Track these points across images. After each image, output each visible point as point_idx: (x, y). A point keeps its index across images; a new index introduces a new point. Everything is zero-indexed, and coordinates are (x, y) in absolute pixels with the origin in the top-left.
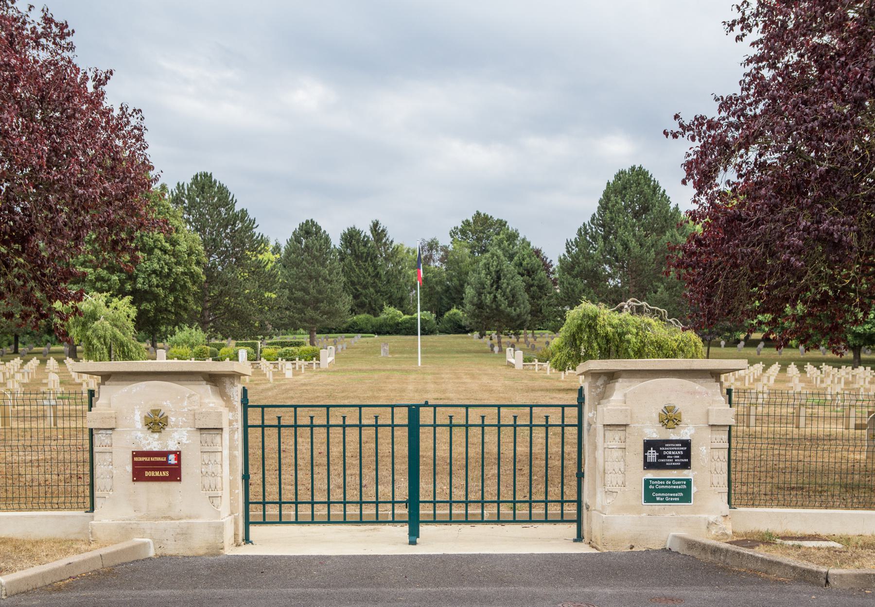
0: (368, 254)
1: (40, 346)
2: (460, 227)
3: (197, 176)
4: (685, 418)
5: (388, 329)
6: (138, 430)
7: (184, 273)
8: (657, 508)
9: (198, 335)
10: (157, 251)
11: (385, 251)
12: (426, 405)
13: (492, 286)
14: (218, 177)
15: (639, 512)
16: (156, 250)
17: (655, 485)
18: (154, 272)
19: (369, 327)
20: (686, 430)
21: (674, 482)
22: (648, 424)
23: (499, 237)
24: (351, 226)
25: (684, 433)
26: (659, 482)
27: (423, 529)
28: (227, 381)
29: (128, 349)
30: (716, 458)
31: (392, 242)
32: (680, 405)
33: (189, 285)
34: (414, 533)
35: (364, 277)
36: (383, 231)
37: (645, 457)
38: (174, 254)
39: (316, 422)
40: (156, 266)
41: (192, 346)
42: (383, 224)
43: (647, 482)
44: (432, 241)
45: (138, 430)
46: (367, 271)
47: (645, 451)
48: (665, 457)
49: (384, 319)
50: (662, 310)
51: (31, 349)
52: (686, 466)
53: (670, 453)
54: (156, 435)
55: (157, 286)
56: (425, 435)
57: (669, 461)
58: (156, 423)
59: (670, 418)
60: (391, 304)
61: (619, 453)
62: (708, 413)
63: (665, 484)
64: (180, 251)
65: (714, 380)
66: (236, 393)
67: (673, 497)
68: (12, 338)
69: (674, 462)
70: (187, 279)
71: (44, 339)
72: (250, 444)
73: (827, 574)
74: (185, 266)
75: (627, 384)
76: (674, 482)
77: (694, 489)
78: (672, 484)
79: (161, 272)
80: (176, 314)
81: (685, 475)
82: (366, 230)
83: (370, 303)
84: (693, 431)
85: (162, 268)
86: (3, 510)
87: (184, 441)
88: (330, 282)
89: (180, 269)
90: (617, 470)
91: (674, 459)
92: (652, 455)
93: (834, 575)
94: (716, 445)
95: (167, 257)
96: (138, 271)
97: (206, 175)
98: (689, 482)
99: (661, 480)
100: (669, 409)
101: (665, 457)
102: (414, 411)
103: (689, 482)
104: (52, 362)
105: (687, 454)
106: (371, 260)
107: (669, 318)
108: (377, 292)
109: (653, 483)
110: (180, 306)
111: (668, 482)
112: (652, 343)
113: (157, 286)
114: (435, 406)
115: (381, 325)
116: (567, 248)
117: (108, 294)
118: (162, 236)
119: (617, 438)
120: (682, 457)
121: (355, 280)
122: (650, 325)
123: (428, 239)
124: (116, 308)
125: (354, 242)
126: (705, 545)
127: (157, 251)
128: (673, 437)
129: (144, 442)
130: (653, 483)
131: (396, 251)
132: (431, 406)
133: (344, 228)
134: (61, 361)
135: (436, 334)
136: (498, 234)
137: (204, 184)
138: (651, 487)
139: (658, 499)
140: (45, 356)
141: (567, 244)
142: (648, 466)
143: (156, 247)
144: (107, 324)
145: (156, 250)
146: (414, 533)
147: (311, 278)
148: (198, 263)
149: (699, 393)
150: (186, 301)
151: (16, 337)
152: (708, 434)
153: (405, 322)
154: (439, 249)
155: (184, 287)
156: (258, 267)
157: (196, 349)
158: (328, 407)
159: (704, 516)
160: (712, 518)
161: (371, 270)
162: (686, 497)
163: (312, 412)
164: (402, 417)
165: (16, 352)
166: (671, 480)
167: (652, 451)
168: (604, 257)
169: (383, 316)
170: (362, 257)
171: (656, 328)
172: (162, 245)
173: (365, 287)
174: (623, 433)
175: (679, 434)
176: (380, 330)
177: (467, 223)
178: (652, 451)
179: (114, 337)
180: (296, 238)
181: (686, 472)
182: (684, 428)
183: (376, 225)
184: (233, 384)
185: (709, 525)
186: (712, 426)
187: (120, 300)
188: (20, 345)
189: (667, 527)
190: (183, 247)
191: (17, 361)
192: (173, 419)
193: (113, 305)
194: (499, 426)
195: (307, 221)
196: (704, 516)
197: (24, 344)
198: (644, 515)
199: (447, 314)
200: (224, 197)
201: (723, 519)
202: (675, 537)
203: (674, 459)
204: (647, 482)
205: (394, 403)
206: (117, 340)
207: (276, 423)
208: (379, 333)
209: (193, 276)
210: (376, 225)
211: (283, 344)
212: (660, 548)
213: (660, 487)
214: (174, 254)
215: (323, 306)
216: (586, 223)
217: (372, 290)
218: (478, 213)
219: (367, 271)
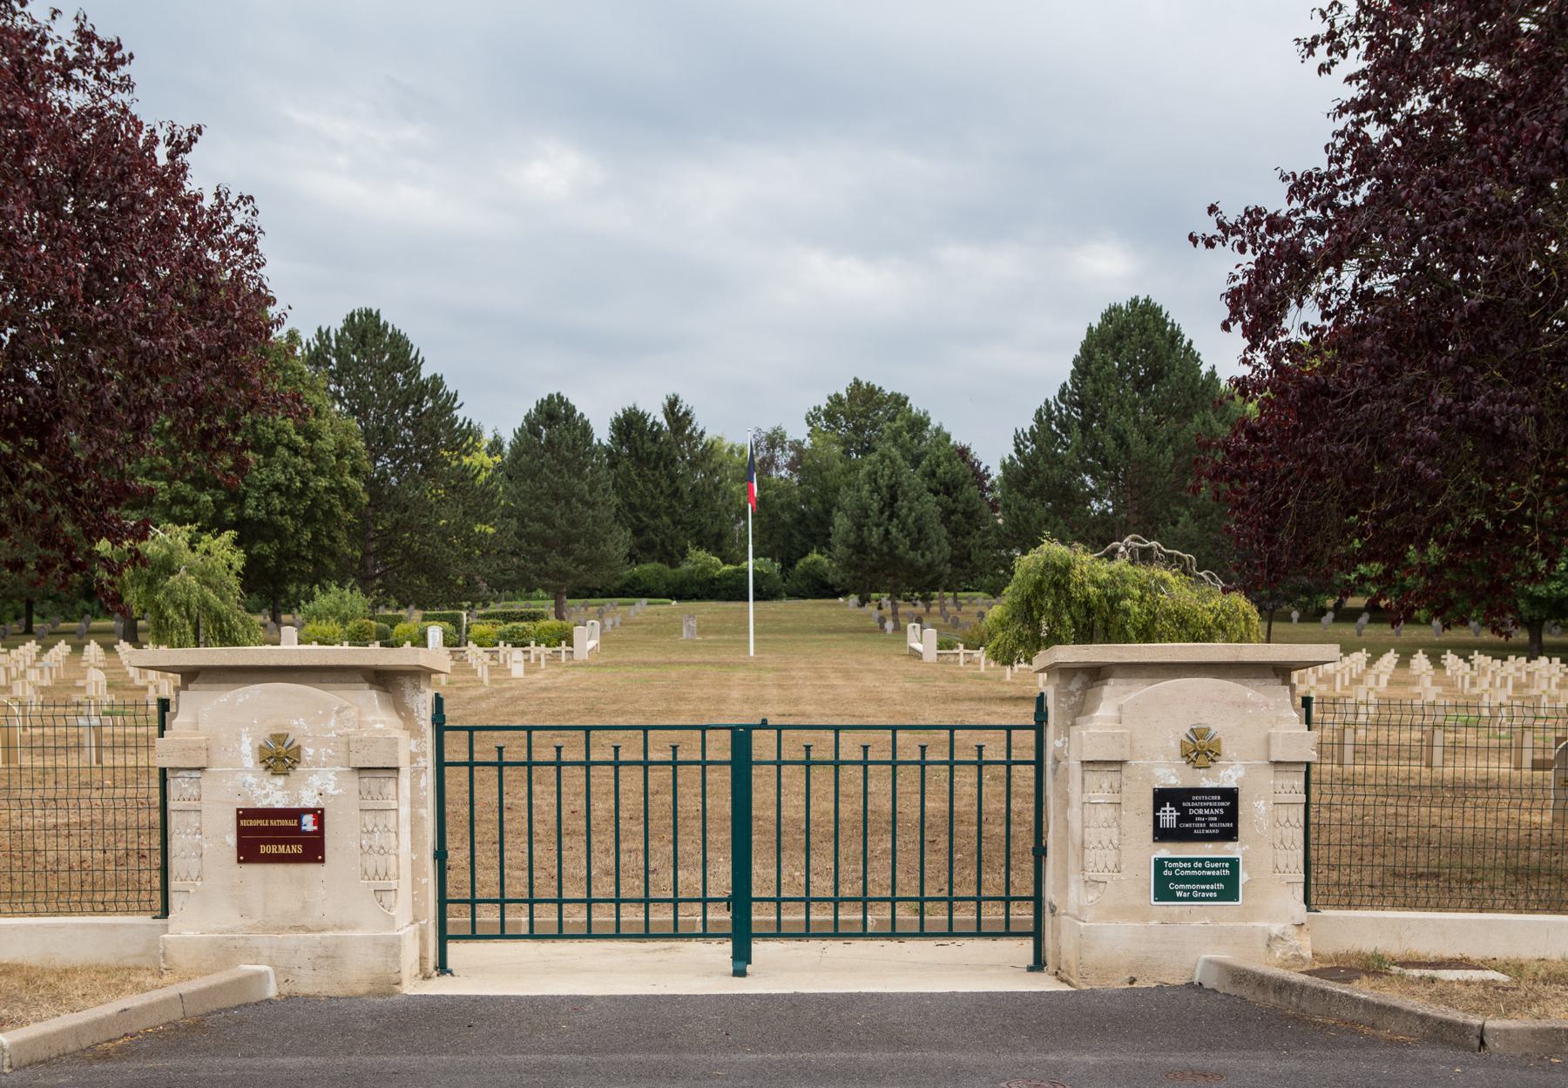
0: (659, 456)
1: (71, 620)
2: (824, 407)
3: (352, 315)
4: (1226, 748)
5: (696, 589)
7: (329, 490)
8: (1177, 910)
9: (355, 600)
10: (282, 452)
11: (691, 451)
12: (764, 725)
13: (881, 512)
14: (392, 318)
15: (1146, 919)
16: (279, 448)
17: (1173, 869)
18: (276, 487)
19: (661, 583)
20: (1229, 772)
22: (1161, 759)
24: (628, 404)
25: (1225, 776)
26: (1181, 865)
27: (759, 948)
28: (407, 684)
29: (229, 625)
30: (1283, 820)
31: (702, 433)
32: (1219, 725)
33: (339, 510)
34: (742, 956)
35: (653, 497)
36: (687, 414)
37: (1156, 820)
38: (313, 456)
40: (280, 477)
41: (344, 620)
42: (686, 403)
43: (1160, 864)
44: (775, 432)
45: (248, 771)
46: (657, 485)
47: (1157, 808)
48: (1192, 819)
49: (690, 572)
51: (55, 625)
52: (1230, 835)
53: (1200, 812)
54: (280, 781)
55: (282, 513)
57: (1199, 827)
59: (1201, 749)
60: (700, 545)
62: (1268, 740)
63: (1192, 868)
64: (322, 450)
65: (1279, 681)
66: (422, 704)
67: (1206, 891)
68: (22, 606)
69: (1208, 827)
70: (335, 500)
71: (78, 608)
72: (447, 796)
73: (1482, 1028)
74: (332, 477)
75: (1124, 688)
77: (1243, 877)
78: (1204, 868)
79: (288, 487)
80: (316, 562)
81: (1228, 852)
82: (656, 413)
83: (663, 544)
84: (1241, 773)
85: (291, 480)
86: (5, 915)
88: (592, 505)
89: (323, 482)
90: (1106, 843)
92: (1169, 816)
93: (1494, 1030)
94: (1283, 798)
95: (299, 460)
96: (248, 485)
97: (369, 313)
98: (1234, 864)
99: (1184, 860)
100: (1198, 733)
101: (1192, 819)
102: (741, 737)
103: (1234, 864)
104: (93, 649)
105: (1232, 814)
106: (666, 466)
107: (1199, 570)
108: (675, 523)
109: (1171, 865)
110: (322, 549)
111: (1197, 865)
112: (1168, 615)
113: (282, 513)
114: (779, 729)
115: (683, 583)
116: (1017, 445)
117: (194, 528)
118: (290, 423)
119: (1105, 786)
120: (1221, 819)
121: (637, 501)
122: (1164, 582)
123: (767, 429)
124: (207, 552)
125: (634, 434)
127: (282, 452)
129: (258, 792)
130: (1171, 865)
131: (710, 450)
133: (616, 409)
134: (108, 648)
135: (781, 598)
136: (892, 419)
137: (365, 330)
138: (1166, 873)
139: (1179, 894)
140: (80, 637)
141: (1017, 437)
143: (279, 442)
144: (192, 581)
145: (279, 448)
146: (742, 956)
147: (556, 498)
148: (355, 472)
149: (1254, 704)
150: (333, 540)
151: (30, 604)
152: (1268, 778)
153: (726, 577)
154: (787, 446)
155: (330, 514)
156: (463, 479)
157: (352, 625)
159: (1261, 924)
160: (1276, 929)
161: (665, 483)
162: (1229, 891)
163: (559, 739)
164: (719, 747)
165: (29, 631)
166: (1203, 860)
167: (1168, 808)
168: (1083, 461)
169: (686, 567)
170: (649, 461)
171: (1175, 588)
172: (291, 440)
173: (655, 515)
175: (1216, 778)
176: (681, 592)
177: (836, 400)
178: (1168, 808)
179: (205, 604)
181: (1229, 846)
182: (1225, 767)
183: (673, 403)
184: (417, 688)
185: (1271, 940)
187: (215, 537)
188: (35, 618)
189: (1197, 943)
190: (328, 442)
191: (31, 647)
192: (311, 751)
193: (202, 546)
194: (894, 764)
195: (551, 397)
196: (1261, 924)
197: (43, 616)
198: (1154, 923)
199: (801, 563)
200: (400, 353)
202: (1209, 962)
203: (1208, 823)
204: (1160, 864)
205: (705, 722)
206: (209, 609)
207: (494, 758)
208: (679, 598)
209: (345, 494)
210: (673, 403)
211: (507, 617)
212: (1183, 982)
213: (1183, 873)
214: (313, 456)
215: (580, 548)
216: (1051, 400)
217: (666, 519)
218: (857, 382)
219: (657, 485)
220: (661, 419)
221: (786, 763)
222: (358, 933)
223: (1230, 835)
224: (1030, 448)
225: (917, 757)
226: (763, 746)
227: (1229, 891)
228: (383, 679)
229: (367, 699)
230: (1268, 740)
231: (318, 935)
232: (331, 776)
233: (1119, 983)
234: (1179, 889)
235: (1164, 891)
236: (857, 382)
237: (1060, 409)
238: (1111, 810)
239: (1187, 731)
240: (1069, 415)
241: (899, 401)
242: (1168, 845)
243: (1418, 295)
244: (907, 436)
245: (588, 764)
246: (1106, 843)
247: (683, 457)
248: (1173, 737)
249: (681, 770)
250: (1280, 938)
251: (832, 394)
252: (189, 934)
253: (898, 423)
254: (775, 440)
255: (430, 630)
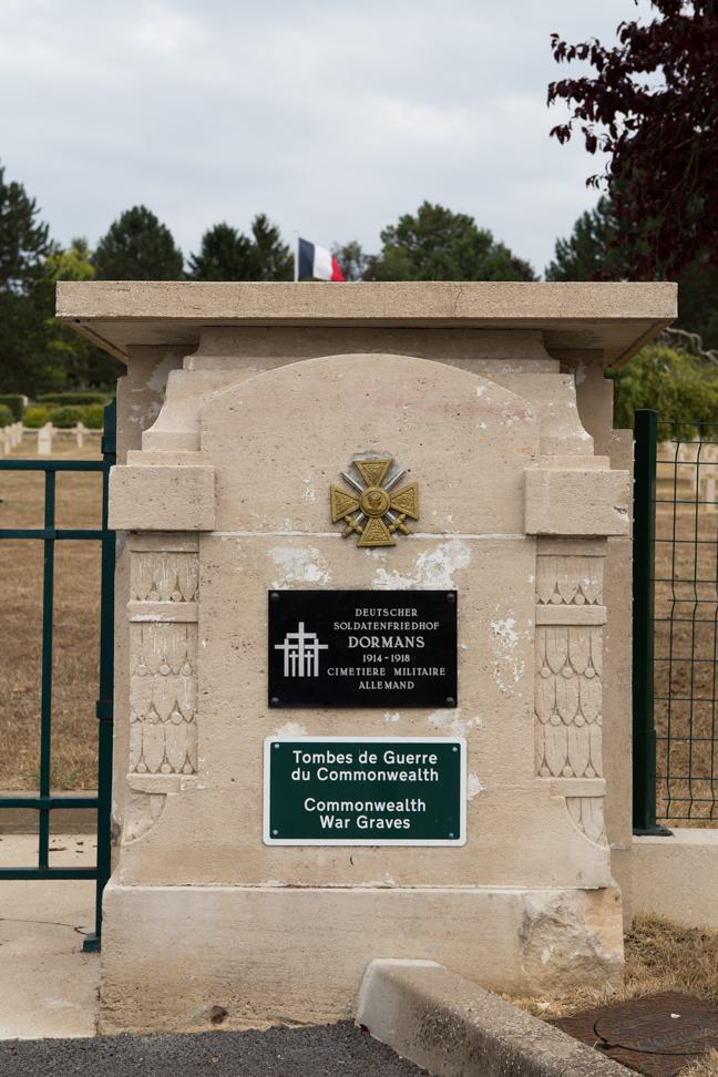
2: (396, 227)
4: (431, 506)
8: (322, 858)
11: (277, 264)
15: (253, 877)
17: (313, 768)
20: (438, 556)
21: (390, 758)
22: (287, 527)
23: (461, 242)
24: (218, 221)
25: (426, 567)
26: (330, 758)
30: (557, 661)
31: (287, 248)
32: (415, 455)
36: (273, 231)
37: (275, 659)
43: (283, 756)
47: (276, 635)
48: (355, 658)
50: (692, 335)
52: (440, 693)
53: (374, 642)
57: (370, 676)
59: (374, 507)
61: (175, 641)
62: (522, 487)
63: (355, 766)
65: (556, 364)
67: (386, 815)
69: (390, 677)
72: (42, 579)
75: (215, 375)
76: (390, 758)
77: (469, 786)
78: (380, 766)
81: (436, 730)
82: (245, 230)
84: (463, 560)
90: (164, 708)
92: (304, 651)
94: (556, 612)
98: (448, 756)
101: (355, 658)
103: (448, 756)
105: (443, 647)
107: (705, 348)
109: (308, 759)
111: (364, 758)
112: (671, 395)
116: (558, 252)
119: (164, 584)
120: (419, 658)
122: (667, 360)
123: (344, 243)
125: (223, 247)
126: (479, 1036)
130: (308, 759)
133: (208, 225)
136: (460, 236)
138: (296, 775)
139: (326, 822)
141: (558, 245)
142: (286, 692)
149: (490, 411)
152: (522, 568)
154: (361, 258)
159: (504, 890)
160: (540, 899)
162: (439, 818)
167: (301, 635)
168: (620, 265)
171: (680, 367)
174: (184, 562)
177: (407, 220)
178: (301, 635)
180: (117, 233)
181: (437, 717)
182: (430, 546)
185: (530, 927)
186: (542, 538)
194: (50, 537)
195: (135, 209)
196: (504, 890)
198: (268, 886)
201: (586, 901)
202: (384, 977)
204: (283, 756)
211: (64, 402)
212: (333, 1018)
213: (334, 776)
216: (590, 211)
218: (427, 205)
220: (253, 239)
223: (440, 693)
224: (571, 256)
227: (439, 818)
230: (522, 487)
233: (190, 1021)
234: (328, 812)
235: (291, 818)
236: (427, 205)
237: (598, 220)
239: (344, 467)
240: (607, 225)
241: (465, 222)
244: (472, 252)
246: (164, 708)
247: (269, 269)
248: (313, 480)
249: (62, 549)
250: (552, 921)
251: (403, 215)
253: (465, 240)
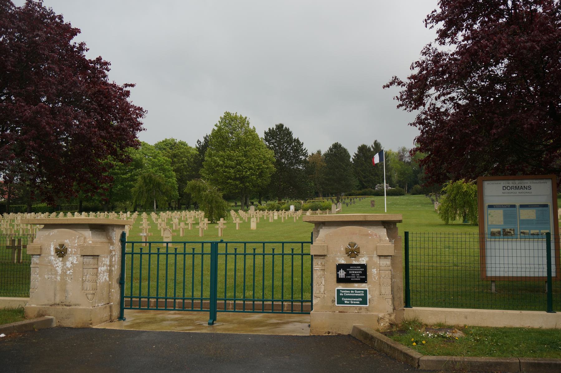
6: (52, 256)
12: (222, 242)
17: (343, 293)
20: (363, 259)
25: (363, 260)
26: (346, 292)
27: (220, 315)
28: (110, 228)
32: (359, 242)
34: (213, 318)
37: (338, 275)
39: (257, 252)
42: (378, 141)
45: (52, 256)
47: (338, 271)
48: (350, 275)
52: (364, 281)
53: (353, 272)
54: (61, 259)
56: (221, 260)
57: (353, 278)
58: (353, 252)
59: (353, 252)
63: (350, 293)
66: (116, 235)
69: (356, 278)
73: (419, 359)
77: (369, 296)
78: (354, 293)
86: (1, 296)
87: (75, 262)
91: (356, 276)
92: (342, 274)
93: (423, 360)
98: (365, 291)
99: (347, 290)
100: (352, 245)
102: (214, 245)
103: (365, 291)
105: (365, 273)
111: (352, 292)
114: (227, 243)
119: (319, 263)
120: (361, 275)
128: (354, 263)
129: (55, 262)
132: (224, 242)
139: (346, 302)
142: (340, 280)
146: (213, 318)
158: (283, 243)
160: (381, 315)
163: (194, 245)
164: (208, 248)
166: (354, 290)
167: (342, 271)
175: (358, 261)
178: (342, 271)
181: (364, 285)
182: (362, 257)
184: (113, 230)
189: (352, 319)
192: (70, 250)
203: (356, 276)
204: (338, 291)
205: (302, 241)
207: (174, 252)
212: (347, 334)
213: (347, 295)
218: (282, 126)
221: (238, 254)
222: (81, 307)
225: (291, 252)
226: (221, 248)
228: (101, 228)
229: (88, 233)
231: (68, 308)
232: (75, 257)
234: (346, 300)
238: (322, 272)
242: (342, 284)
243: (443, 78)
245: (283, 255)
249: (187, 256)
252: (33, 305)
254: (404, 150)
255: (522, 218)
